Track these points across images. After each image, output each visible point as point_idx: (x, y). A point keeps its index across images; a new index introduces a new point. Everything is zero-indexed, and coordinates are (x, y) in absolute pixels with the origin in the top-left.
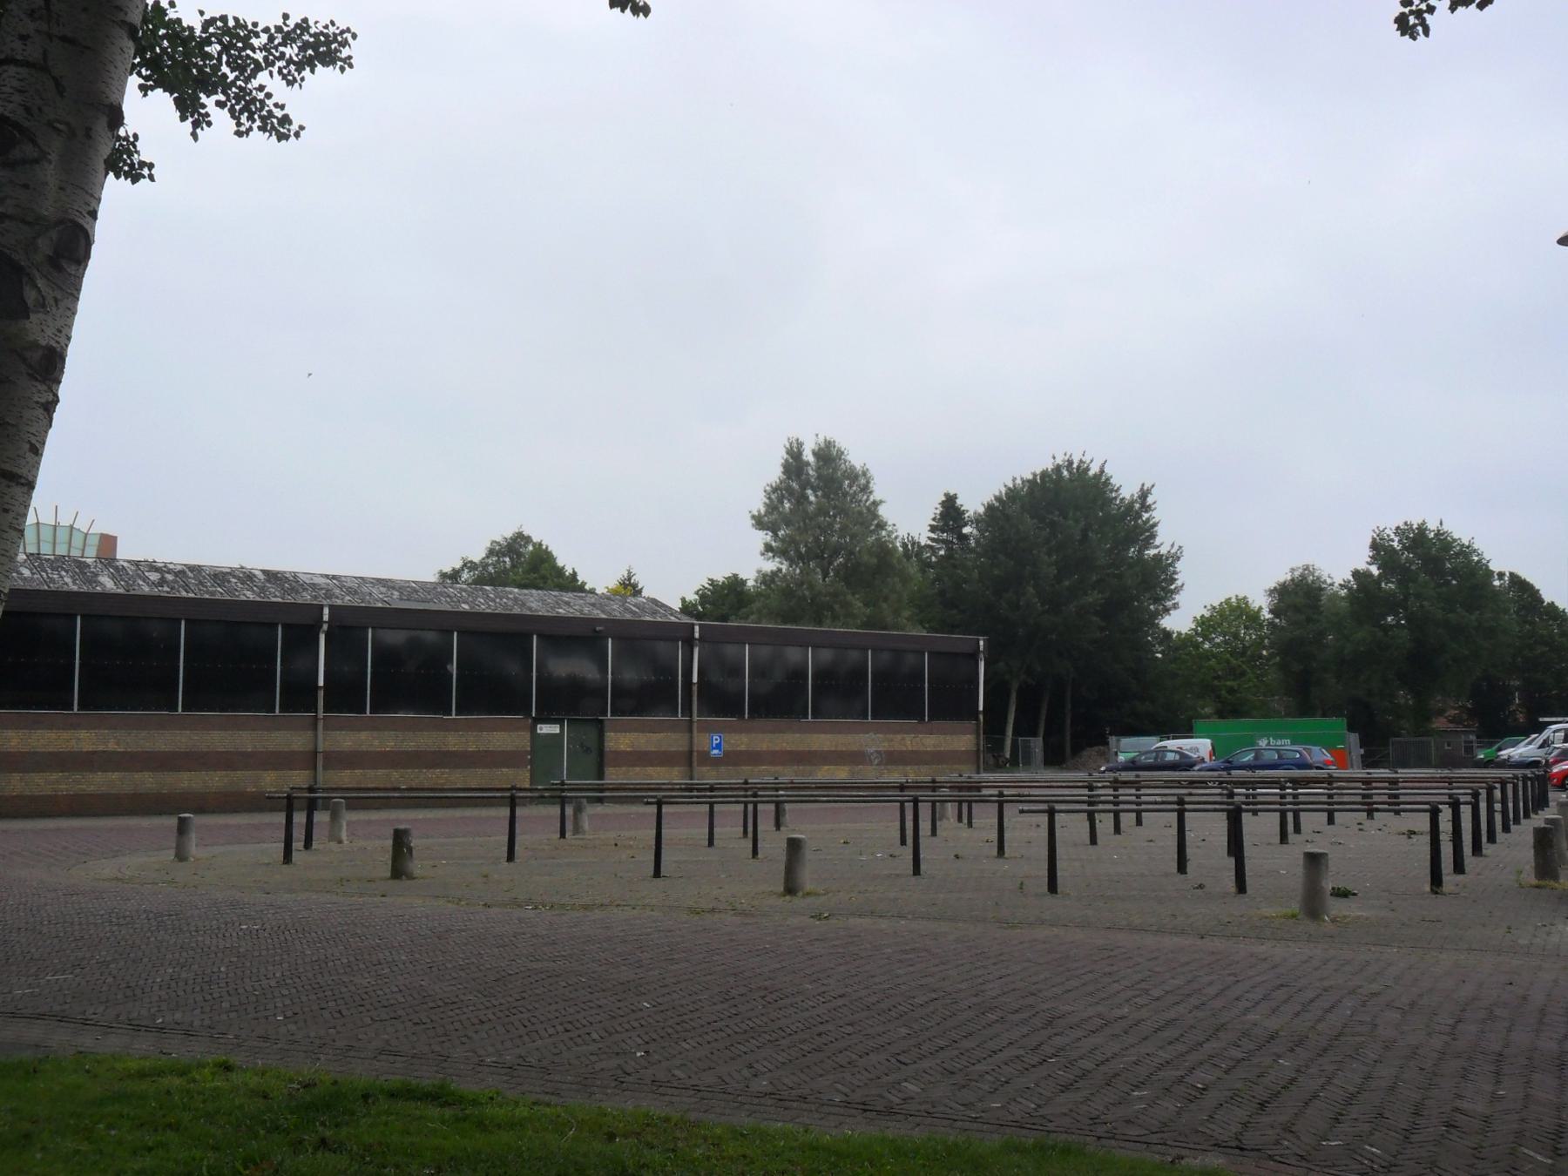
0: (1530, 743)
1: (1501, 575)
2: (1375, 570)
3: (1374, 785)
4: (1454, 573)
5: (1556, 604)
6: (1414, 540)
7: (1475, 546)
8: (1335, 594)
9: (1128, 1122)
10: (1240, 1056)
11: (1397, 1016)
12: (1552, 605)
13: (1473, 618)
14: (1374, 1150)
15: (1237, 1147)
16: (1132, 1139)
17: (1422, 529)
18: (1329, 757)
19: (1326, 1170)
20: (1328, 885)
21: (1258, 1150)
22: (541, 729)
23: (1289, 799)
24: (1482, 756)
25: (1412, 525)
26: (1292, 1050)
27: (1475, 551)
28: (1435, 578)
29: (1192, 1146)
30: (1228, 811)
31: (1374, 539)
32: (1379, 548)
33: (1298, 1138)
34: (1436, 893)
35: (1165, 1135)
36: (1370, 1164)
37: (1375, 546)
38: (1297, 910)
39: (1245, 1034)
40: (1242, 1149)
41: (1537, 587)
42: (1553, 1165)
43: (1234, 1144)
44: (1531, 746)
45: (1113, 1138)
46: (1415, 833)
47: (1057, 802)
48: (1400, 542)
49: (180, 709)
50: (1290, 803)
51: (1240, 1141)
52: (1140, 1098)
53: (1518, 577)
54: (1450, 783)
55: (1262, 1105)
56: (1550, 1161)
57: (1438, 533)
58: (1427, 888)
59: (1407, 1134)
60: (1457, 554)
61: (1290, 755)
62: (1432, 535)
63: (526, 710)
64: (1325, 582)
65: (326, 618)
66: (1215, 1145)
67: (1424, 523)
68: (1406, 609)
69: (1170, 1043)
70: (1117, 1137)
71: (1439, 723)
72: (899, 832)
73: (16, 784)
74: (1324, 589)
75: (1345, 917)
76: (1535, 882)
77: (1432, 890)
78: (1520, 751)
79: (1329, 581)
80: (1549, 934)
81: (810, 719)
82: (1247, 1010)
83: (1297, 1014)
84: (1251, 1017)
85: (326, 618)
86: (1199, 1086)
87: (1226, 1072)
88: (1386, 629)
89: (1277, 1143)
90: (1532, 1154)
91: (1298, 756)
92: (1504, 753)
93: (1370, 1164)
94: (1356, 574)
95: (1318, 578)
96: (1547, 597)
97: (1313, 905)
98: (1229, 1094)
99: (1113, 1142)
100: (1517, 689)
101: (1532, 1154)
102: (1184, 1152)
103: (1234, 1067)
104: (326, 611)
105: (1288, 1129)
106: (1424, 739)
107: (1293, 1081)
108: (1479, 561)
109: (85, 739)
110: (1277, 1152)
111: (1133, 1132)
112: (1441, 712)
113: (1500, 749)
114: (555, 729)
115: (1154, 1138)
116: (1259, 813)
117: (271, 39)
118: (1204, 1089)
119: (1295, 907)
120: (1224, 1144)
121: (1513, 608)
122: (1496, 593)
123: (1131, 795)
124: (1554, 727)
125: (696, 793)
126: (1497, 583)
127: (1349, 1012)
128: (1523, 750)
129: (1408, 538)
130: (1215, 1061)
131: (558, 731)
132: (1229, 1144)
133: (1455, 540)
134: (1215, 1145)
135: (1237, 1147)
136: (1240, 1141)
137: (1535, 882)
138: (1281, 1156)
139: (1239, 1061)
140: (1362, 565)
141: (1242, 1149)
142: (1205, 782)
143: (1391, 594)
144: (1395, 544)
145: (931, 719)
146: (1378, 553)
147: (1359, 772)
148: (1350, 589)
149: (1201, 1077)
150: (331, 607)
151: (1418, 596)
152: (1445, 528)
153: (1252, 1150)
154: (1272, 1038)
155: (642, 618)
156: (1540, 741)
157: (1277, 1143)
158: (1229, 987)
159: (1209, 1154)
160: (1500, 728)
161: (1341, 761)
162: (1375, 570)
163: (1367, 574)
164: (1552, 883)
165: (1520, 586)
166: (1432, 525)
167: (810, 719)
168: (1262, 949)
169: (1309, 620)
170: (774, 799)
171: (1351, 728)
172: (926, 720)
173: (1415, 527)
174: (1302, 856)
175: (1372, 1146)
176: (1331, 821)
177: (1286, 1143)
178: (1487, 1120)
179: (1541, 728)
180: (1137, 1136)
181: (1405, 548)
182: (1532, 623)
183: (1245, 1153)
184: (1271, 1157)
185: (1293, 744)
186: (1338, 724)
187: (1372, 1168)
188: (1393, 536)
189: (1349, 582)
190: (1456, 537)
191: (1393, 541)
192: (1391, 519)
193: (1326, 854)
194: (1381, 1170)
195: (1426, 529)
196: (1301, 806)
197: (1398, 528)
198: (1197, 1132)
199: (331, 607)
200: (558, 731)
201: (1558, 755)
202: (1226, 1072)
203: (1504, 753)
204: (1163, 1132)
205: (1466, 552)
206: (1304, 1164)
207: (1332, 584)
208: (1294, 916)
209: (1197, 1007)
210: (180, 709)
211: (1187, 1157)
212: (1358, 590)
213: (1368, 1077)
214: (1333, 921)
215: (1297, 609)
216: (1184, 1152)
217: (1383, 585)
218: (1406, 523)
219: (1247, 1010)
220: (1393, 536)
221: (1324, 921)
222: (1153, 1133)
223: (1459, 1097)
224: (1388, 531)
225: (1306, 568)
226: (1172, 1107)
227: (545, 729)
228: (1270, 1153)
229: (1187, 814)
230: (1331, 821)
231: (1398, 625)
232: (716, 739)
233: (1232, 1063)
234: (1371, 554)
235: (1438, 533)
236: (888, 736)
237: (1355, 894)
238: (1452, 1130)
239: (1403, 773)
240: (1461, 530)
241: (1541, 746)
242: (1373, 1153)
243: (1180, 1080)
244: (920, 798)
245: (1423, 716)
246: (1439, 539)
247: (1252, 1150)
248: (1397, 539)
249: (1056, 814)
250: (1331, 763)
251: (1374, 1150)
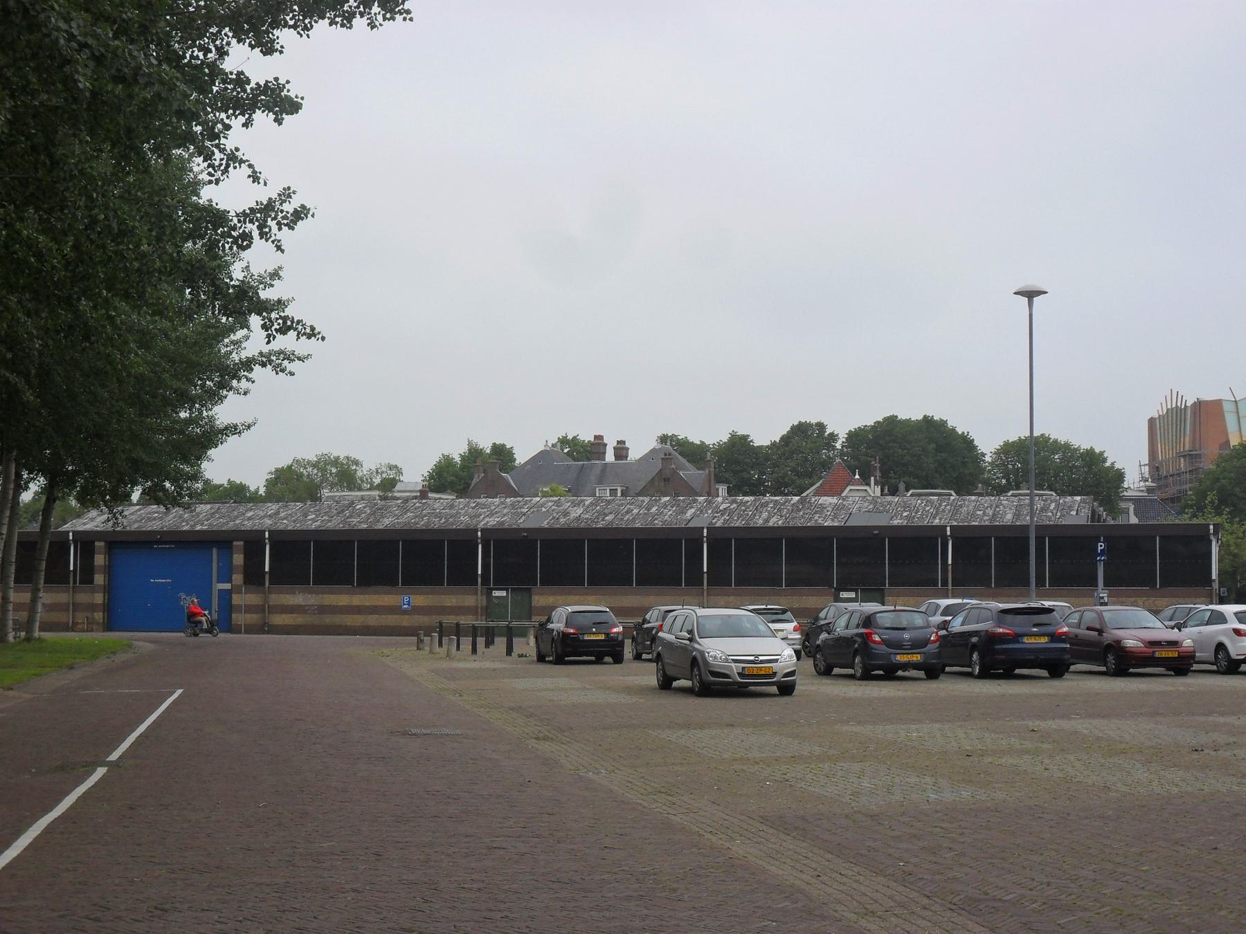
22: (842, 595)
28: (927, 440)
47: (136, 640)
49: (634, 585)
63: (831, 586)
65: (705, 534)
81: (784, 587)
85: (705, 534)
104: (948, 529)
109: (358, 599)
114: (504, 593)
117: (211, 274)
131: (505, 595)
145: (358, 585)
150: (74, 532)
155: (360, 527)
167: (784, 587)
172: (993, 586)
199: (74, 532)
200: (505, 595)
210: (634, 585)
227: (497, 593)
229: (655, 664)
232: (406, 599)
236: (1120, 599)
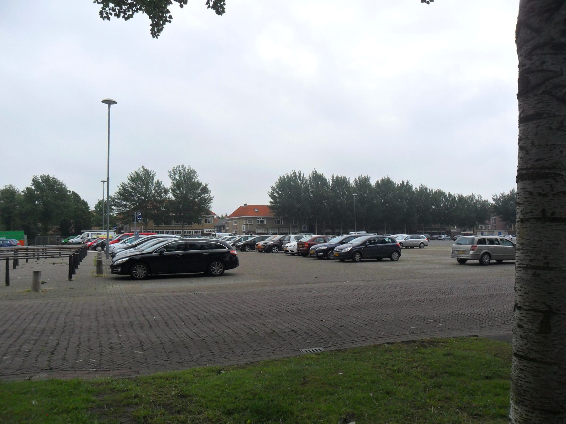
0: (78, 237)
1: (70, 192)
2: (33, 188)
3: (47, 250)
4: (57, 190)
5: (85, 200)
6: (46, 180)
7: (64, 183)
8: (20, 194)
9: (6, 368)
10: (36, 338)
11: (78, 318)
12: (83, 200)
13: (62, 203)
14: (93, 360)
15: (50, 369)
16: (10, 374)
17: (48, 177)
18: (18, 242)
19: (81, 370)
20: (40, 281)
21: (57, 368)
23: (36, 254)
24: (63, 241)
25: (45, 175)
26: (52, 334)
27: (63, 184)
29: (33, 372)
30: (69, 257)
31: (33, 178)
32: (35, 181)
33: (68, 361)
34: (70, 280)
35: (22, 370)
36: (94, 365)
37: (33, 181)
38: (30, 289)
39: (34, 331)
40: (52, 369)
41: (79, 195)
42: (144, 354)
43: (49, 368)
44: (78, 238)
45: (3, 375)
46: (55, 263)
48: (42, 180)
50: (36, 256)
51: (50, 366)
52: (7, 359)
53: (74, 192)
54: (60, 249)
55: (52, 353)
56: (143, 353)
57: (53, 179)
58: (68, 279)
59: (101, 353)
60: (58, 185)
61: (6, 242)
62: (51, 179)
64: (16, 190)
66: (42, 370)
67: (49, 175)
68: (42, 200)
69: (9, 338)
70: (4, 375)
71: (51, 232)
72: (5, 271)
73: (1, 256)
74: (16, 192)
75: (46, 290)
76: (97, 275)
77: (69, 279)
78: (75, 240)
79: (18, 190)
80: (106, 289)
82: (30, 323)
83: (48, 322)
84: (32, 325)
86: (27, 351)
87: (34, 345)
88: (36, 205)
89: (62, 364)
90: (137, 352)
91: (9, 242)
92: (71, 240)
93: (94, 365)
94: (27, 188)
95: (14, 189)
96: (82, 198)
97: (36, 287)
98: (39, 351)
99: (3, 377)
100: (73, 223)
101: (137, 352)
102: (32, 374)
103: (36, 342)
105: (64, 359)
106: (47, 237)
107: (58, 343)
108: (65, 187)
110: (64, 368)
111: (10, 371)
112: (51, 229)
113: (69, 239)
115: (18, 372)
116: (40, 259)
118: (29, 352)
119: (30, 288)
120: (45, 369)
121: (73, 200)
122: (69, 197)
123: (12, 254)
124: (85, 233)
125: (44, 256)
126: (68, 194)
127: (64, 319)
128: (76, 239)
129: (44, 179)
130: (28, 341)
132: (46, 369)
133: (58, 181)
134: (42, 370)
135: (50, 369)
136: (50, 366)
137: (97, 275)
138: (66, 368)
139: (36, 340)
140: (29, 186)
141: (52, 369)
142: (3, 251)
143: (38, 195)
144: (40, 180)
146: (34, 183)
147: (25, 247)
148: (25, 193)
149: (26, 348)
151: (46, 196)
152: (55, 177)
153: (55, 369)
154: (44, 330)
156: (81, 237)
157: (62, 364)
158: (19, 316)
159: (40, 373)
160: (67, 233)
161: (22, 243)
162: (33, 188)
163: (31, 189)
164: (102, 275)
165: (75, 195)
166: (51, 176)
168: (22, 302)
169: (11, 201)
170: (26, 257)
171: (25, 234)
173: (46, 176)
174: (32, 274)
175: (92, 359)
176: (27, 261)
177: (65, 364)
178: (121, 344)
179: (81, 233)
180: (12, 373)
181: (43, 182)
182: (78, 205)
183: (53, 370)
184: (62, 370)
185: (6, 239)
186: (21, 233)
187: (95, 366)
188: (39, 178)
189: (25, 190)
190: (58, 180)
191: (39, 179)
192: (39, 173)
193: (40, 271)
194: (97, 366)
195: (50, 177)
196: (29, 257)
197: (41, 176)
198: (34, 367)
201: (87, 240)
202: (34, 345)
203: (71, 240)
204: (21, 369)
205: (61, 184)
206: (73, 369)
207: (18, 191)
208: (29, 291)
209: (12, 324)
211: (34, 376)
212: (28, 193)
213: (80, 338)
214: (42, 291)
215: (7, 198)
216: (32, 374)
217: (36, 192)
218: (43, 175)
219: (30, 323)
220: (39, 178)
221: (40, 292)
222: (17, 370)
223: (109, 339)
224: (38, 177)
225: (11, 186)
226: (20, 360)
228: (61, 368)
230: (27, 261)
231: (39, 204)
233: (34, 341)
234: (32, 183)
235: (53, 179)
237: (46, 283)
238: (113, 349)
239: (48, 246)
240: (60, 178)
241: (81, 238)
242: (93, 361)
243: (19, 350)
244: (10, 258)
245: (46, 230)
246: (53, 180)
247: (55, 369)
248: (40, 179)
249: (9, 260)
250: (19, 244)
251: (93, 360)
